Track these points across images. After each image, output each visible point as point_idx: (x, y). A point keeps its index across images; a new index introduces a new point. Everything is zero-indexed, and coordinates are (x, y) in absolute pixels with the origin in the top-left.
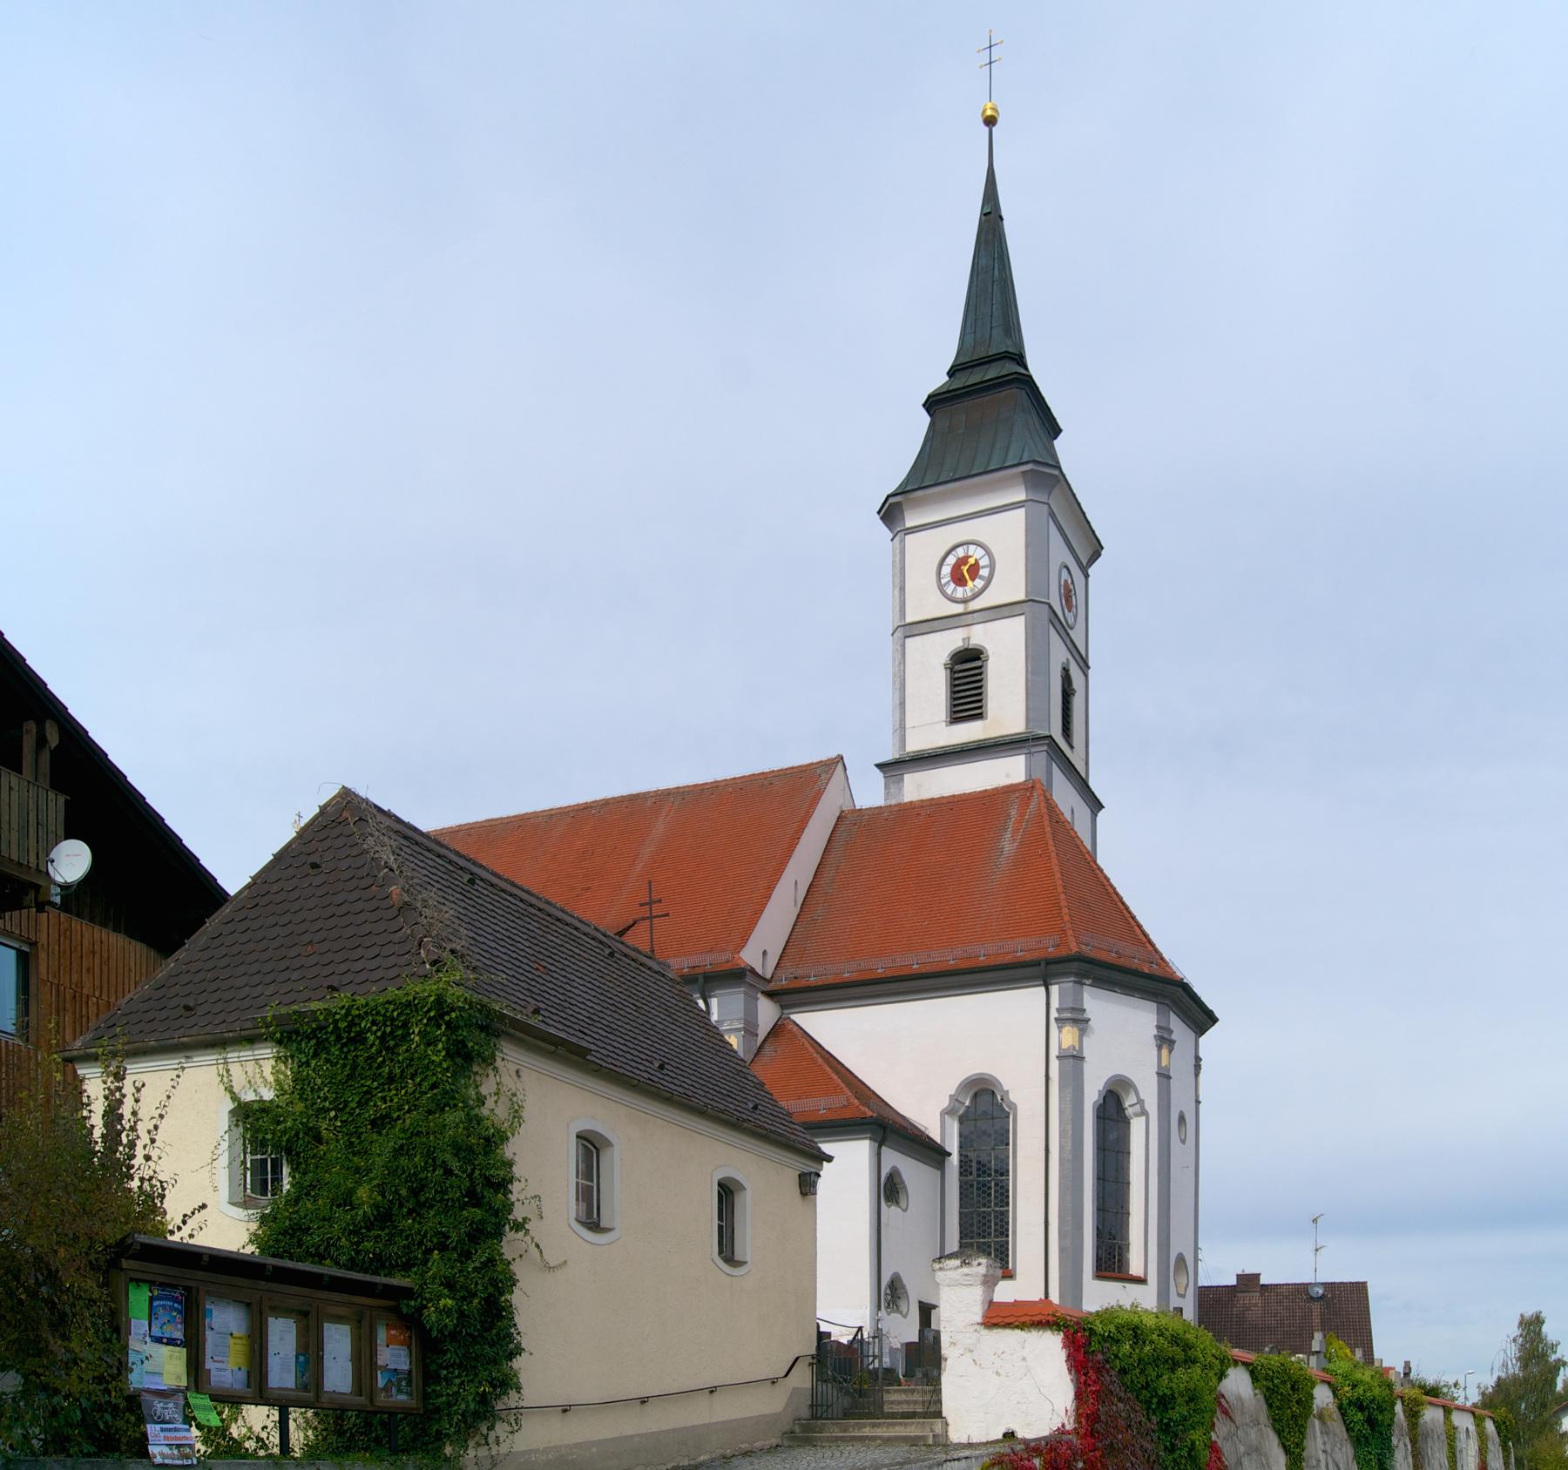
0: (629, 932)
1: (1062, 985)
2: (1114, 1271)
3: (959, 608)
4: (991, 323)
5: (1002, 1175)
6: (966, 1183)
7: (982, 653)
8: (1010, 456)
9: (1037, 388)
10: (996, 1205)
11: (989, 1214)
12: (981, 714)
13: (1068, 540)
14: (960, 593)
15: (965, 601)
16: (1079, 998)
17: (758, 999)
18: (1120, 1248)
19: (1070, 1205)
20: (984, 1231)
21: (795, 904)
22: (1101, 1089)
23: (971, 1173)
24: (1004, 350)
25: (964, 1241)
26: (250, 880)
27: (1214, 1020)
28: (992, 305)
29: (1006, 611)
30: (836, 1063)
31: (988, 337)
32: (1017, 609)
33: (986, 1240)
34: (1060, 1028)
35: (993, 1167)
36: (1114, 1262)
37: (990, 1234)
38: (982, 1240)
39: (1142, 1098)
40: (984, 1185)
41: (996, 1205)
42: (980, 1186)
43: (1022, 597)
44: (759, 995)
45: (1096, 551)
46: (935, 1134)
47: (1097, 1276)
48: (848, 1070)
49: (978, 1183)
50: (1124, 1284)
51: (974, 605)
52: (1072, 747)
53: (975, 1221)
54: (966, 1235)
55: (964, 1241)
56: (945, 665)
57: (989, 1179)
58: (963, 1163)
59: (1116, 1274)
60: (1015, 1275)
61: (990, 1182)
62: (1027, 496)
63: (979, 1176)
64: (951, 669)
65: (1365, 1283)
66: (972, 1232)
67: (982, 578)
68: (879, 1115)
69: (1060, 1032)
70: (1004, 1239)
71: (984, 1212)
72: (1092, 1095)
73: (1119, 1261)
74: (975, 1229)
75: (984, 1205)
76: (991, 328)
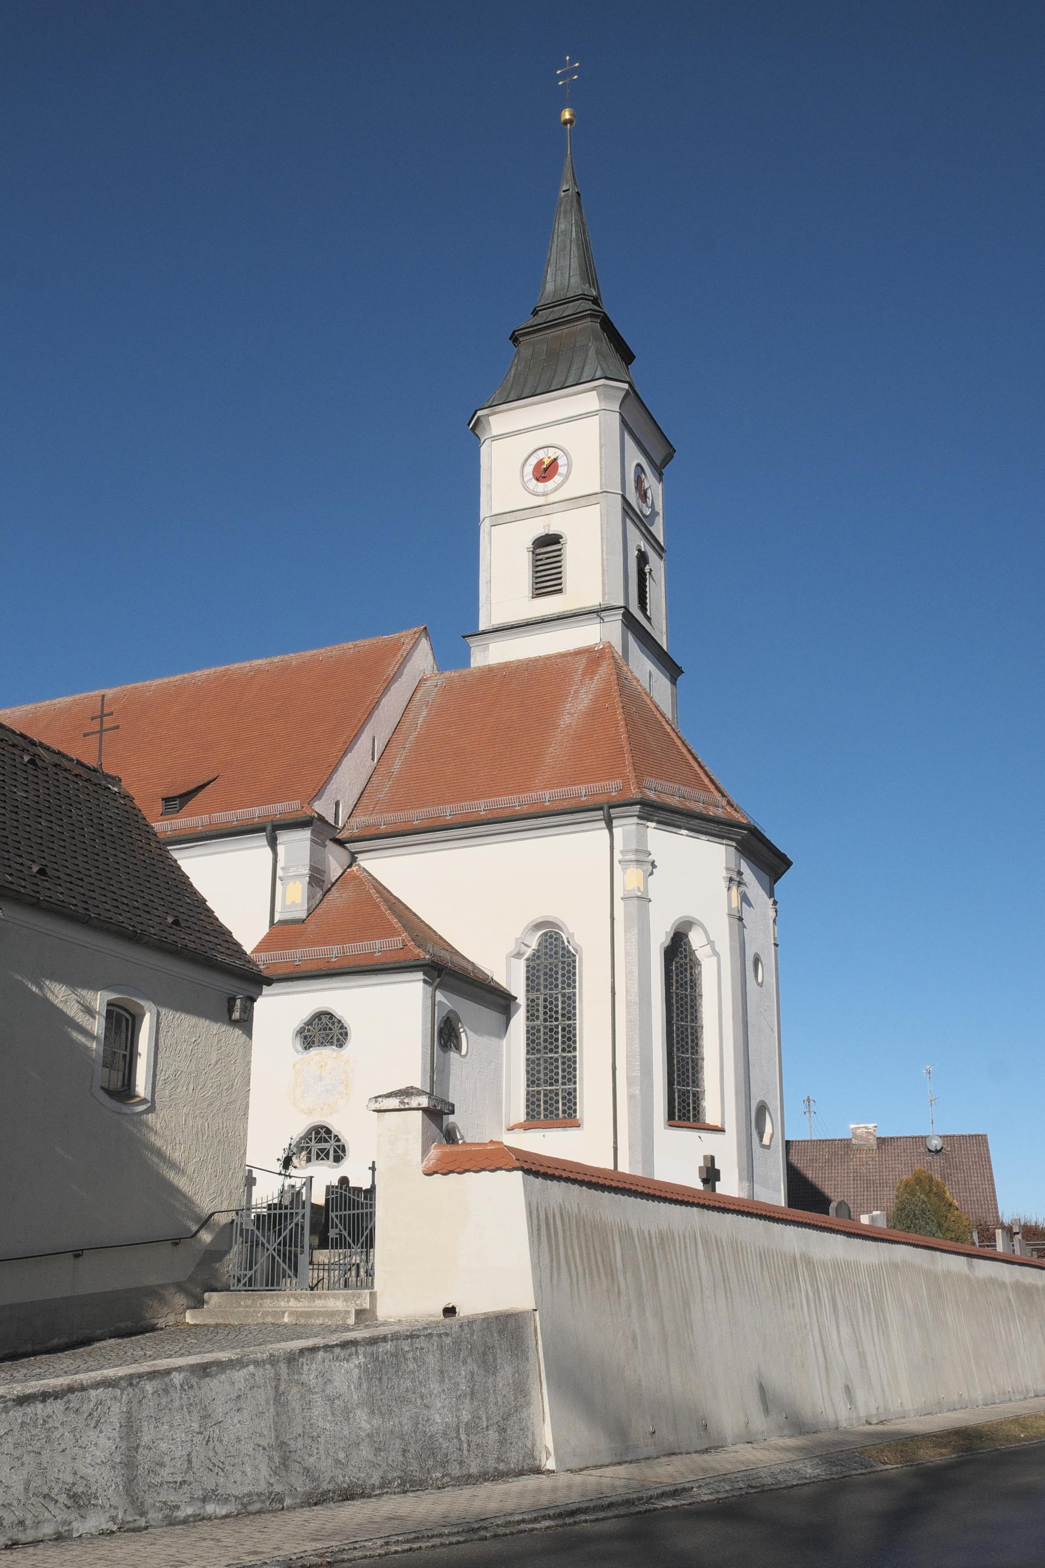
0: (209, 786)
1: (626, 827)
2: (689, 1120)
3: (541, 501)
4: (569, 273)
5: (569, 1019)
6: (533, 1028)
7: (562, 538)
8: (585, 374)
9: (612, 323)
10: (564, 1050)
11: (557, 1060)
12: (561, 590)
13: (653, 460)
14: (541, 487)
15: (545, 494)
16: (642, 839)
17: (325, 846)
18: (694, 1095)
19: (638, 1050)
20: (551, 1078)
21: (373, 759)
22: (669, 930)
23: (538, 1018)
24: (581, 292)
25: (531, 1089)
26: (694, 949)
27: (788, 864)
28: (570, 259)
29: (583, 501)
30: (402, 907)
31: (567, 284)
32: (592, 500)
33: (553, 1088)
34: (624, 870)
35: (560, 1011)
36: (689, 1110)
37: (557, 1081)
38: (549, 1088)
39: (712, 939)
40: (551, 1030)
41: (564, 1050)
42: (547, 1030)
43: (598, 490)
44: (328, 842)
45: (671, 452)
46: (500, 978)
47: (670, 1126)
48: (415, 915)
49: (545, 1027)
50: (701, 1134)
51: (552, 498)
52: (649, 619)
53: (542, 1067)
54: (533, 1082)
55: (531, 1089)
56: (527, 548)
57: (556, 1023)
58: (530, 1008)
59: (691, 1123)
60: (583, 1124)
61: (557, 1027)
62: (600, 406)
63: (545, 1020)
64: (533, 552)
65: (985, 1136)
66: (539, 1079)
67: (560, 475)
68: (433, 955)
69: (625, 873)
70: (572, 1086)
71: (551, 1058)
72: (660, 938)
73: (694, 1109)
74: (542, 1075)
75: (551, 1051)
76: (569, 277)
